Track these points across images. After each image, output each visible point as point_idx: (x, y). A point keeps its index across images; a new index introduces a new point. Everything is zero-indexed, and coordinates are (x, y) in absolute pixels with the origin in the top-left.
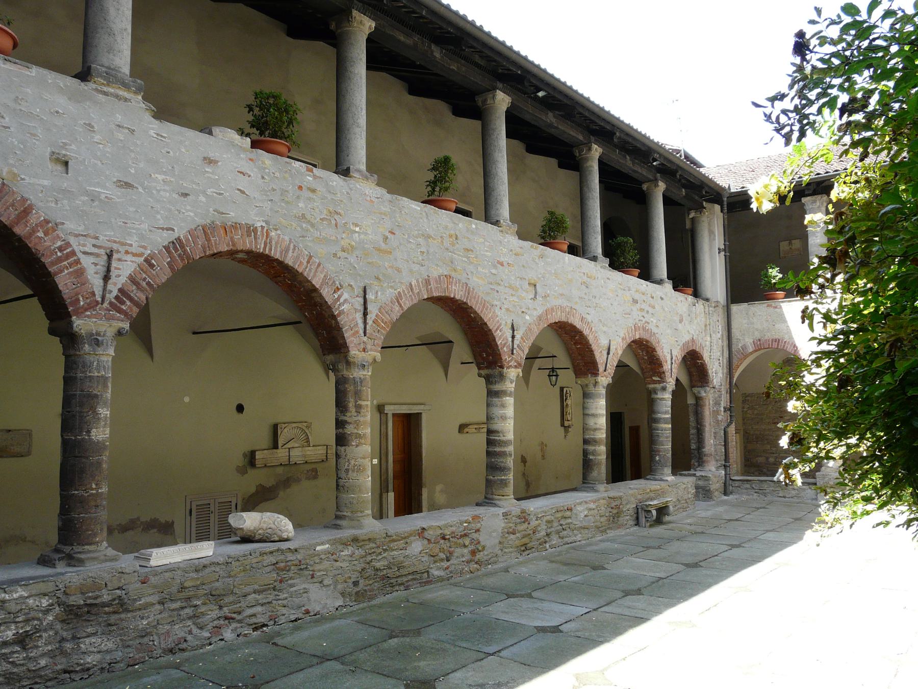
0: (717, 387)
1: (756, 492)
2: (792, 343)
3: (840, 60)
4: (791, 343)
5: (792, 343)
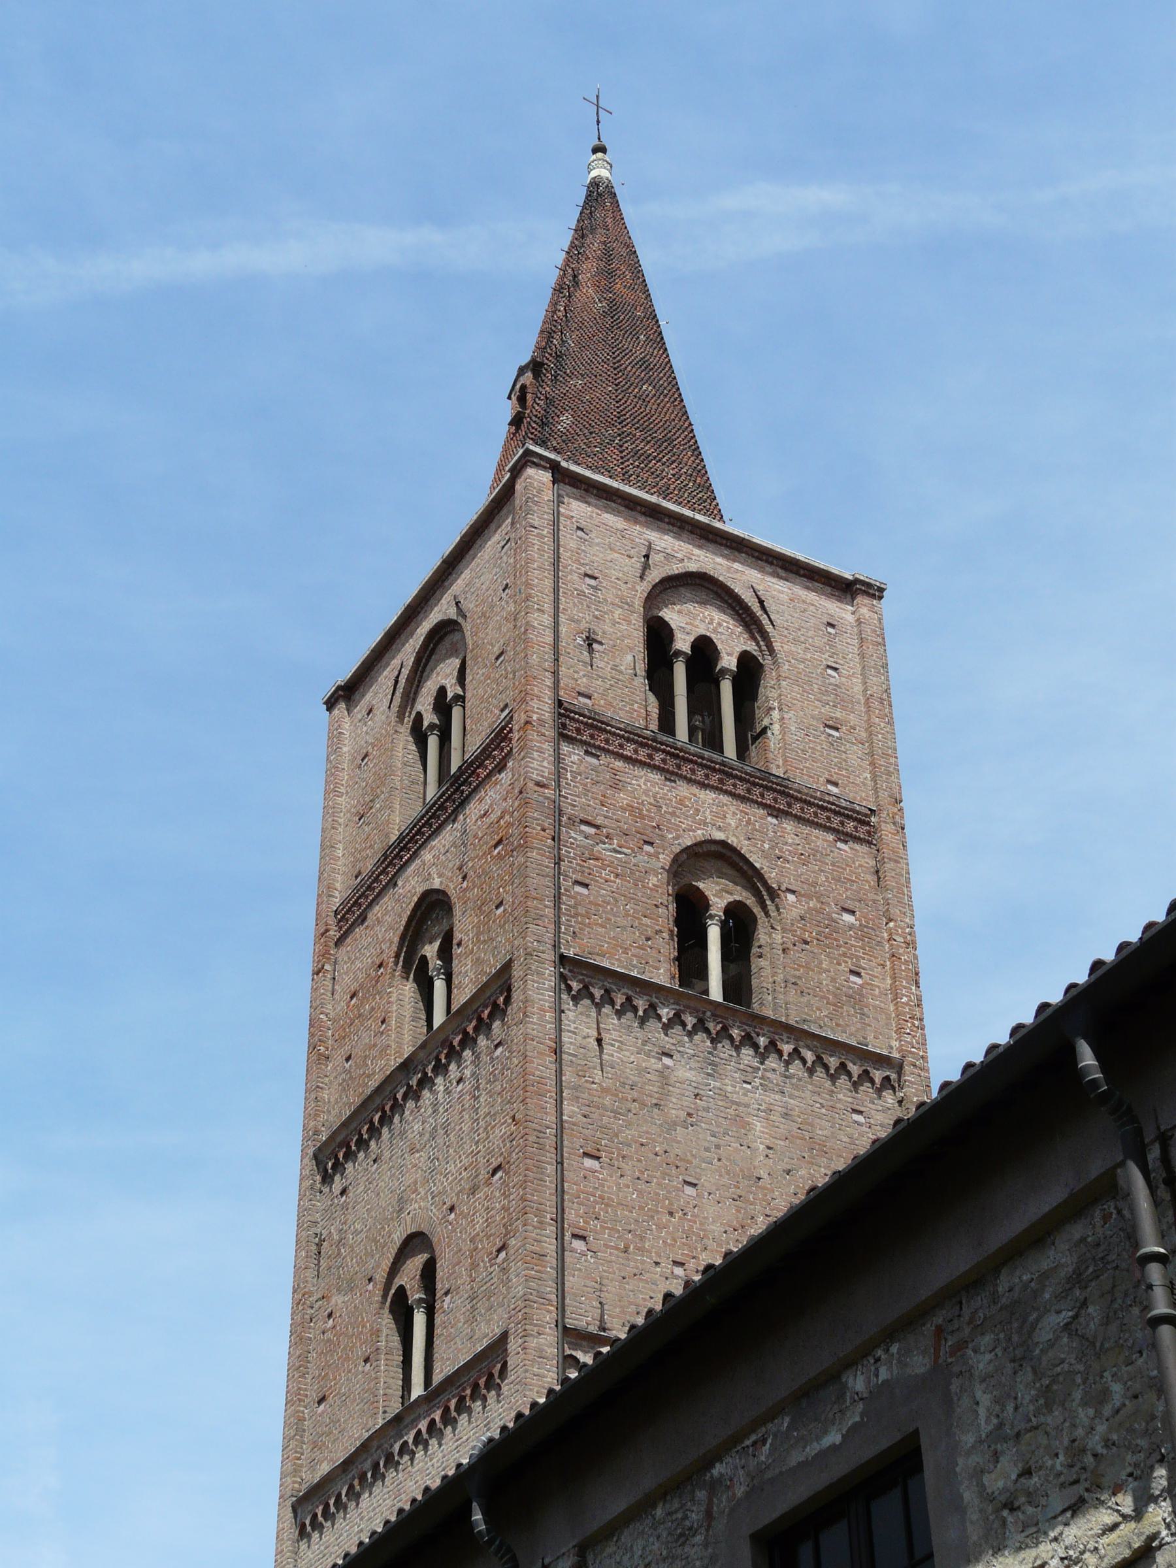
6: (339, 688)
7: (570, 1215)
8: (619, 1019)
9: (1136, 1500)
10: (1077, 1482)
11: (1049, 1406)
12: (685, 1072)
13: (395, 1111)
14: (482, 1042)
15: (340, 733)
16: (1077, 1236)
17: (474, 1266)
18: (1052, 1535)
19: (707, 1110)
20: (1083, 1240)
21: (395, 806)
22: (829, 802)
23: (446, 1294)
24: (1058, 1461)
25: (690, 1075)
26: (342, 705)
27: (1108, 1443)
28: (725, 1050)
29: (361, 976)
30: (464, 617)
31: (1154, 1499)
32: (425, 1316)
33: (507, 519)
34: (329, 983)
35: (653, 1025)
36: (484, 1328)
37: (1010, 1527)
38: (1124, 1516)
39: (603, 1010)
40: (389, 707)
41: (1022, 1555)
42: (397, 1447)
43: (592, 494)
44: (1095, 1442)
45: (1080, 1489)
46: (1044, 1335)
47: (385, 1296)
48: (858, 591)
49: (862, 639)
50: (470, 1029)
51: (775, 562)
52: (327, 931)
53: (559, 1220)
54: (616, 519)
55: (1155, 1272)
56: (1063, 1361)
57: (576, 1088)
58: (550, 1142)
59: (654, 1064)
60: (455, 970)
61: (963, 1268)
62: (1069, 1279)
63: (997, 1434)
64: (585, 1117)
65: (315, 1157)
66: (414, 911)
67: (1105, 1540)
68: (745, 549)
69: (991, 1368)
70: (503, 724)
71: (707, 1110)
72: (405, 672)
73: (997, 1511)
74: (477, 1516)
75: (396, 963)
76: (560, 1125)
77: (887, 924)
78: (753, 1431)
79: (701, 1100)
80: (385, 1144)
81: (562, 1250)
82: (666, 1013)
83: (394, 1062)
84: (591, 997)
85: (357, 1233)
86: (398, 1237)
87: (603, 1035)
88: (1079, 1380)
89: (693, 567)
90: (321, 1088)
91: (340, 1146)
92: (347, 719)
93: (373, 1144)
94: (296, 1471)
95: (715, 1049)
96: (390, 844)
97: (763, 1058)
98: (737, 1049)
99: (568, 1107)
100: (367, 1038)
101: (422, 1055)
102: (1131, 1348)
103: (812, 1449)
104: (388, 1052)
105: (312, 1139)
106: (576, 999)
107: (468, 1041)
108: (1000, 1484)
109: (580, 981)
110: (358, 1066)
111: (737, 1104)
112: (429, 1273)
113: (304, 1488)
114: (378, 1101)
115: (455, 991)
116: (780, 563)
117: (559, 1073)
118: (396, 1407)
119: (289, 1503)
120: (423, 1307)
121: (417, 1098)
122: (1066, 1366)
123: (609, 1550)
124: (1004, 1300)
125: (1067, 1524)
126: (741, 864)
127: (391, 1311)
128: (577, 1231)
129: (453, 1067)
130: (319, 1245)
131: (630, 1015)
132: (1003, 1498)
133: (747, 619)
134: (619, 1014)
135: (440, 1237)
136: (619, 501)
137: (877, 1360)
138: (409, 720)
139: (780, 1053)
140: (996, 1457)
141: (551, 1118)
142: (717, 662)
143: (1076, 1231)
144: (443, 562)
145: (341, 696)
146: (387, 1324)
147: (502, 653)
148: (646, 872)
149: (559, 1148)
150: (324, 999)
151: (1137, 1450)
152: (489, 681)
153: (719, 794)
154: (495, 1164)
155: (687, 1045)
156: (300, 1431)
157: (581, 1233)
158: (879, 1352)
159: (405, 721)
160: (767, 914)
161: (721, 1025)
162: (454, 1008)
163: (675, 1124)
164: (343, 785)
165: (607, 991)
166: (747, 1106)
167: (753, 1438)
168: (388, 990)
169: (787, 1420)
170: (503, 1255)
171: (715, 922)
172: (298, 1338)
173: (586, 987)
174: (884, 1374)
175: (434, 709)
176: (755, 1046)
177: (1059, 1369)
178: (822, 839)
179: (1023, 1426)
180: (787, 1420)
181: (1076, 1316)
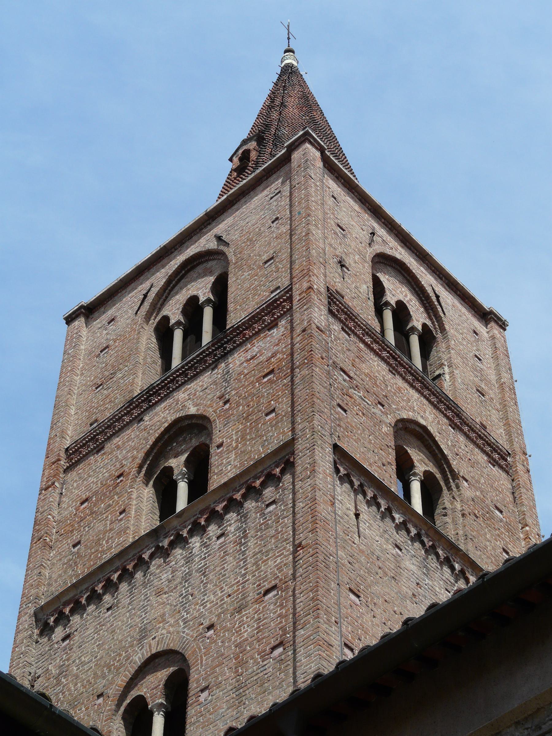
6: (82, 307)
8: (368, 507)
13: (137, 569)
15: (80, 335)
21: (139, 374)
22: (484, 434)
26: (82, 319)
30: (227, 244)
32: (164, 719)
33: (277, 180)
39: (358, 496)
40: (136, 313)
43: (340, 182)
47: (119, 706)
48: (492, 320)
49: (496, 347)
51: (444, 278)
52: (59, 460)
54: (354, 204)
64: (350, 563)
66: (167, 430)
68: (427, 262)
70: (277, 297)
72: (155, 290)
75: (139, 472)
77: (522, 528)
79: (420, 588)
89: (398, 256)
90: (45, 567)
92: (85, 329)
95: (427, 558)
96: (134, 396)
104: (128, 531)
105: (33, 602)
116: (447, 281)
120: (163, 711)
126: (434, 448)
127: (123, 718)
133: (427, 305)
136: (356, 194)
138: (154, 322)
142: (409, 323)
144: (206, 214)
145: (82, 313)
147: (272, 258)
148: (380, 421)
150: (53, 505)
152: (256, 277)
153: (421, 397)
155: (410, 547)
159: (151, 322)
160: (449, 489)
161: (432, 543)
164: (79, 369)
168: (129, 491)
171: (417, 478)
175: (182, 312)
176: (452, 568)
178: (482, 458)
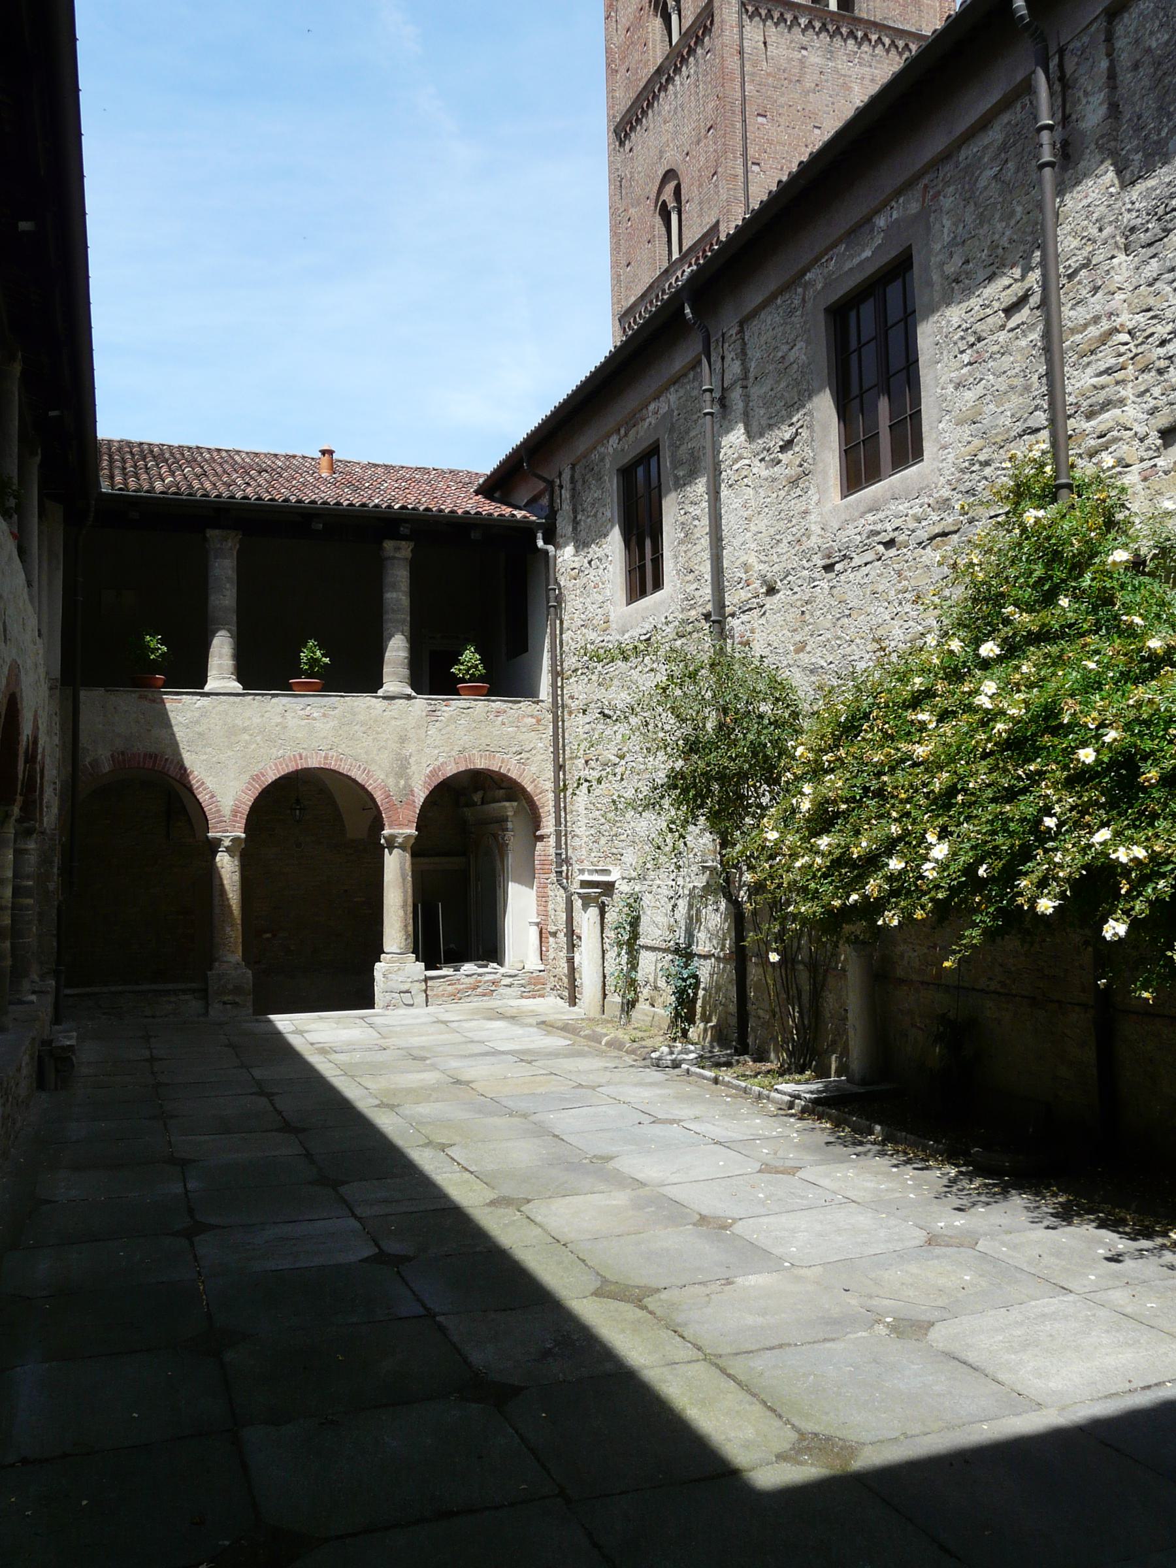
0: (48, 831)
1: (104, 1014)
2: (178, 763)
3: (820, 390)
4: (175, 761)
5: (178, 763)
7: (751, 152)
9: (1023, 270)
10: (992, 264)
11: (981, 224)
12: (814, 58)
14: (699, 51)
16: (1006, 121)
17: (701, 185)
18: (977, 294)
19: (827, 81)
20: (1009, 123)
23: (687, 202)
24: (984, 254)
25: (818, 60)
27: (1011, 241)
28: (838, 42)
29: (632, 17)
31: (1032, 269)
34: (614, 24)
35: (796, 30)
36: (707, 219)
37: (956, 292)
38: (1016, 280)
41: (961, 305)
42: (667, 286)
44: (1004, 242)
45: (993, 268)
46: (982, 183)
47: (656, 206)
50: (692, 44)
53: (745, 154)
55: (1045, 136)
56: (991, 197)
57: (753, 74)
58: (738, 109)
59: (798, 56)
60: (682, 7)
61: (940, 148)
62: (999, 148)
63: (953, 243)
65: (615, 131)
67: (1004, 294)
69: (952, 206)
71: (827, 81)
73: (950, 284)
74: (687, 311)
75: (650, 7)
76: (744, 97)
78: (826, 254)
80: (649, 121)
81: (746, 172)
82: (803, 21)
83: (652, 71)
84: (760, 15)
85: (639, 173)
86: (661, 173)
87: (768, 40)
88: (999, 207)
91: (627, 124)
93: (644, 120)
94: (619, 302)
97: (860, 45)
98: (845, 41)
99: (748, 87)
100: (637, 56)
101: (666, 63)
102: (1029, 185)
103: (856, 261)
106: (751, 18)
107: (691, 51)
108: (953, 269)
109: (753, 6)
110: (633, 75)
111: (845, 76)
112: (677, 191)
113: (624, 309)
114: (645, 94)
115: (683, 21)
117: (743, 66)
118: (666, 265)
119: (617, 318)
121: (666, 90)
122: (992, 200)
123: (755, 323)
124: (962, 165)
125: (985, 287)
127: (660, 214)
128: (755, 161)
129: (684, 68)
130: (621, 182)
131: (782, 25)
132: (953, 277)
134: (776, 24)
135: (682, 171)
137: (892, 208)
139: (870, 41)
140: (951, 255)
141: (739, 95)
143: (1005, 118)
146: (658, 221)
149: (743, 112)
151: (1025, 243)
154: (709, 126)
156: (619, 281)
157: (757, 161)
158: (893, 203)
162: (683, 31)
163: (809, 92)
165: (769, 11)
166: (850, 77)
167: (826, 257)
169: (844, 246)
170: (715, 178)
172: (614, 234)
173: (757, 9)
174: (895, 216)
176: (856, 38)
177: (988, 202)
179: (967, 236)
180: (844, 246)
181: (1001, 169)
